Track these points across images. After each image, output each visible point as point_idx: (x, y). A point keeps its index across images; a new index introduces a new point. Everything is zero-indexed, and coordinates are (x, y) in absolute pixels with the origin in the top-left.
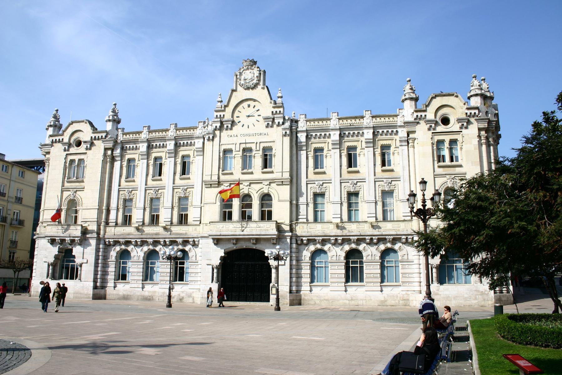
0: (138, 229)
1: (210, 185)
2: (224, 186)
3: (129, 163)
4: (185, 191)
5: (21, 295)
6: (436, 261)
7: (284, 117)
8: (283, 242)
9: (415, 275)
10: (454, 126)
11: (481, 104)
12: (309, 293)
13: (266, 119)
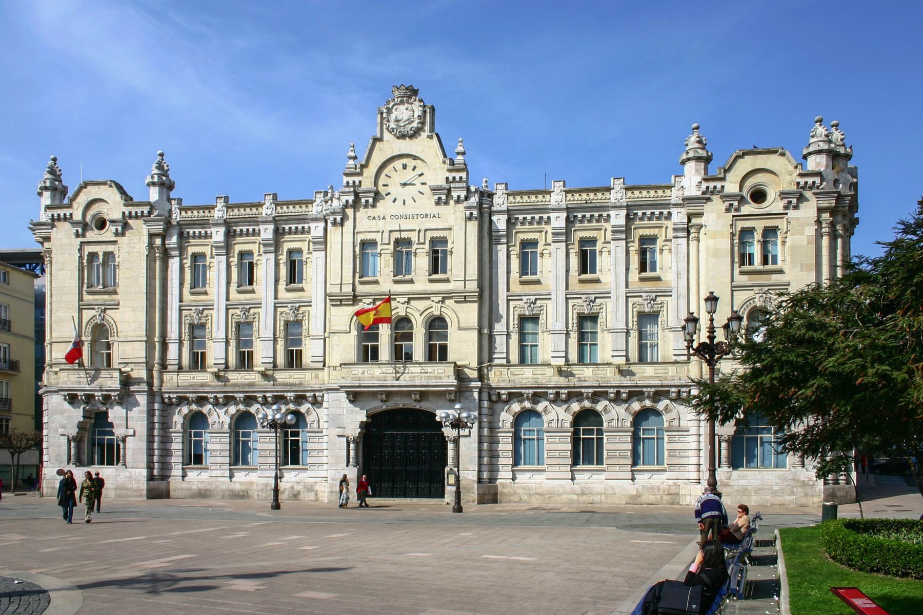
0: (217, 376)
1: (338, 301)
2: (364, 303)
3: (195, 262)
4: (296, 311)
5: (26, 494)
6: (728, 429)
7: (469, 187)
8: (466, 398)
9: (691, 453)
10: (773, 204)
11: (827, 167)
12: (511, 483)
13: (435, 189)
